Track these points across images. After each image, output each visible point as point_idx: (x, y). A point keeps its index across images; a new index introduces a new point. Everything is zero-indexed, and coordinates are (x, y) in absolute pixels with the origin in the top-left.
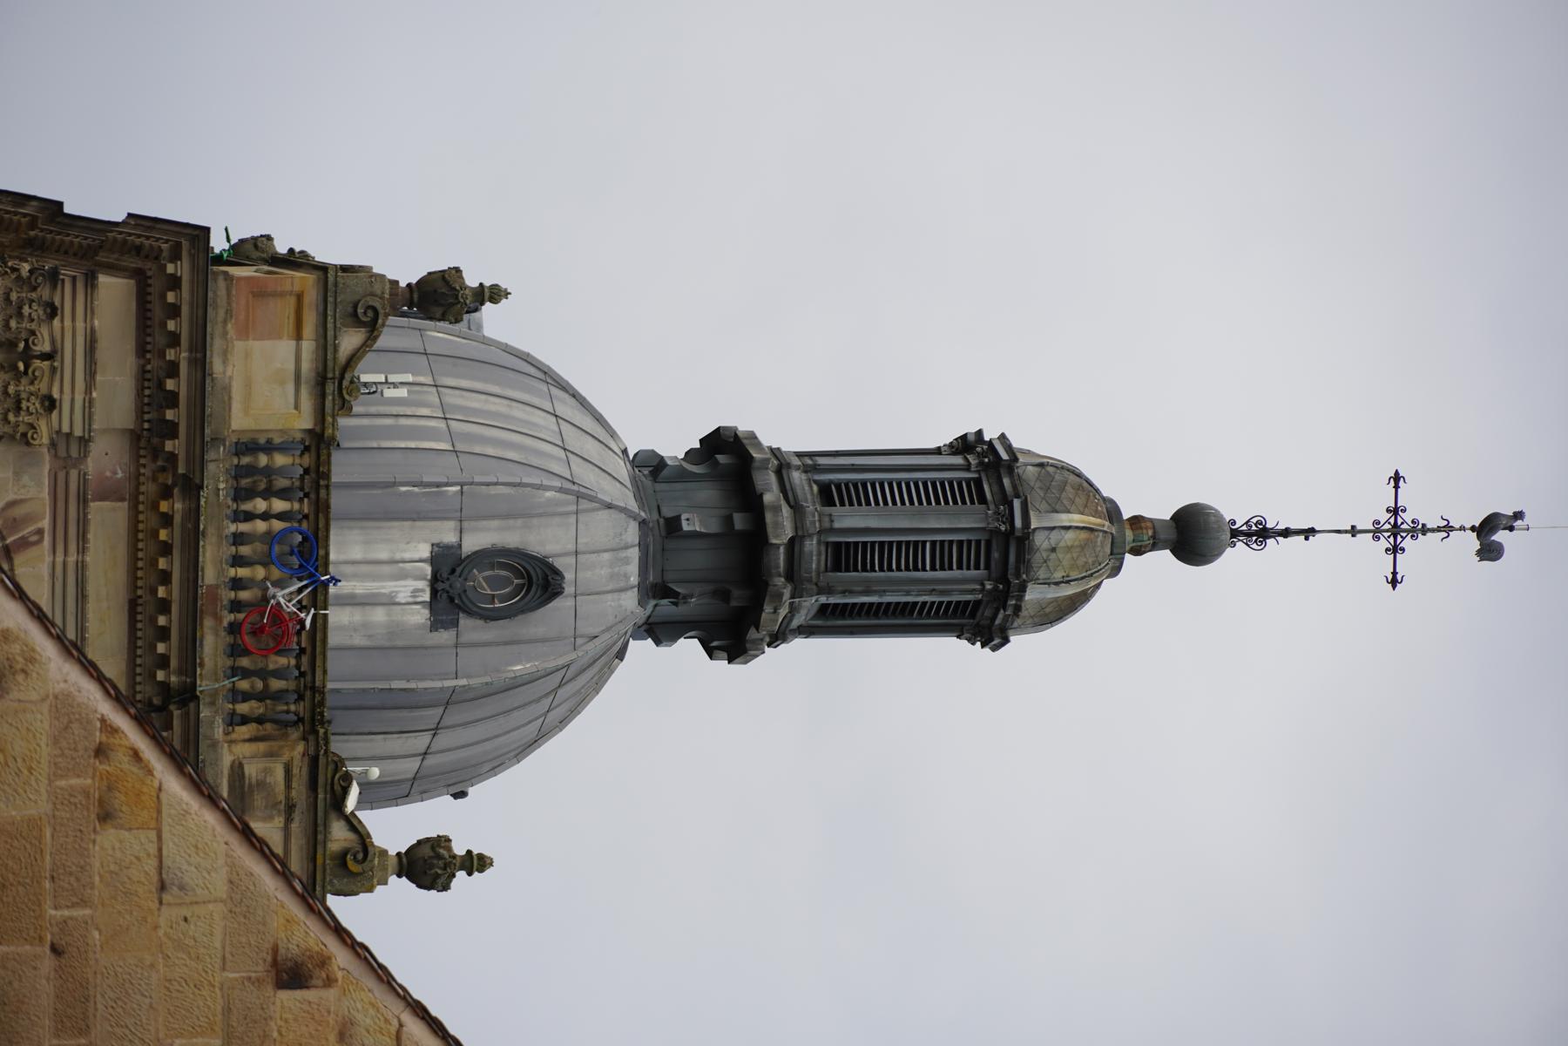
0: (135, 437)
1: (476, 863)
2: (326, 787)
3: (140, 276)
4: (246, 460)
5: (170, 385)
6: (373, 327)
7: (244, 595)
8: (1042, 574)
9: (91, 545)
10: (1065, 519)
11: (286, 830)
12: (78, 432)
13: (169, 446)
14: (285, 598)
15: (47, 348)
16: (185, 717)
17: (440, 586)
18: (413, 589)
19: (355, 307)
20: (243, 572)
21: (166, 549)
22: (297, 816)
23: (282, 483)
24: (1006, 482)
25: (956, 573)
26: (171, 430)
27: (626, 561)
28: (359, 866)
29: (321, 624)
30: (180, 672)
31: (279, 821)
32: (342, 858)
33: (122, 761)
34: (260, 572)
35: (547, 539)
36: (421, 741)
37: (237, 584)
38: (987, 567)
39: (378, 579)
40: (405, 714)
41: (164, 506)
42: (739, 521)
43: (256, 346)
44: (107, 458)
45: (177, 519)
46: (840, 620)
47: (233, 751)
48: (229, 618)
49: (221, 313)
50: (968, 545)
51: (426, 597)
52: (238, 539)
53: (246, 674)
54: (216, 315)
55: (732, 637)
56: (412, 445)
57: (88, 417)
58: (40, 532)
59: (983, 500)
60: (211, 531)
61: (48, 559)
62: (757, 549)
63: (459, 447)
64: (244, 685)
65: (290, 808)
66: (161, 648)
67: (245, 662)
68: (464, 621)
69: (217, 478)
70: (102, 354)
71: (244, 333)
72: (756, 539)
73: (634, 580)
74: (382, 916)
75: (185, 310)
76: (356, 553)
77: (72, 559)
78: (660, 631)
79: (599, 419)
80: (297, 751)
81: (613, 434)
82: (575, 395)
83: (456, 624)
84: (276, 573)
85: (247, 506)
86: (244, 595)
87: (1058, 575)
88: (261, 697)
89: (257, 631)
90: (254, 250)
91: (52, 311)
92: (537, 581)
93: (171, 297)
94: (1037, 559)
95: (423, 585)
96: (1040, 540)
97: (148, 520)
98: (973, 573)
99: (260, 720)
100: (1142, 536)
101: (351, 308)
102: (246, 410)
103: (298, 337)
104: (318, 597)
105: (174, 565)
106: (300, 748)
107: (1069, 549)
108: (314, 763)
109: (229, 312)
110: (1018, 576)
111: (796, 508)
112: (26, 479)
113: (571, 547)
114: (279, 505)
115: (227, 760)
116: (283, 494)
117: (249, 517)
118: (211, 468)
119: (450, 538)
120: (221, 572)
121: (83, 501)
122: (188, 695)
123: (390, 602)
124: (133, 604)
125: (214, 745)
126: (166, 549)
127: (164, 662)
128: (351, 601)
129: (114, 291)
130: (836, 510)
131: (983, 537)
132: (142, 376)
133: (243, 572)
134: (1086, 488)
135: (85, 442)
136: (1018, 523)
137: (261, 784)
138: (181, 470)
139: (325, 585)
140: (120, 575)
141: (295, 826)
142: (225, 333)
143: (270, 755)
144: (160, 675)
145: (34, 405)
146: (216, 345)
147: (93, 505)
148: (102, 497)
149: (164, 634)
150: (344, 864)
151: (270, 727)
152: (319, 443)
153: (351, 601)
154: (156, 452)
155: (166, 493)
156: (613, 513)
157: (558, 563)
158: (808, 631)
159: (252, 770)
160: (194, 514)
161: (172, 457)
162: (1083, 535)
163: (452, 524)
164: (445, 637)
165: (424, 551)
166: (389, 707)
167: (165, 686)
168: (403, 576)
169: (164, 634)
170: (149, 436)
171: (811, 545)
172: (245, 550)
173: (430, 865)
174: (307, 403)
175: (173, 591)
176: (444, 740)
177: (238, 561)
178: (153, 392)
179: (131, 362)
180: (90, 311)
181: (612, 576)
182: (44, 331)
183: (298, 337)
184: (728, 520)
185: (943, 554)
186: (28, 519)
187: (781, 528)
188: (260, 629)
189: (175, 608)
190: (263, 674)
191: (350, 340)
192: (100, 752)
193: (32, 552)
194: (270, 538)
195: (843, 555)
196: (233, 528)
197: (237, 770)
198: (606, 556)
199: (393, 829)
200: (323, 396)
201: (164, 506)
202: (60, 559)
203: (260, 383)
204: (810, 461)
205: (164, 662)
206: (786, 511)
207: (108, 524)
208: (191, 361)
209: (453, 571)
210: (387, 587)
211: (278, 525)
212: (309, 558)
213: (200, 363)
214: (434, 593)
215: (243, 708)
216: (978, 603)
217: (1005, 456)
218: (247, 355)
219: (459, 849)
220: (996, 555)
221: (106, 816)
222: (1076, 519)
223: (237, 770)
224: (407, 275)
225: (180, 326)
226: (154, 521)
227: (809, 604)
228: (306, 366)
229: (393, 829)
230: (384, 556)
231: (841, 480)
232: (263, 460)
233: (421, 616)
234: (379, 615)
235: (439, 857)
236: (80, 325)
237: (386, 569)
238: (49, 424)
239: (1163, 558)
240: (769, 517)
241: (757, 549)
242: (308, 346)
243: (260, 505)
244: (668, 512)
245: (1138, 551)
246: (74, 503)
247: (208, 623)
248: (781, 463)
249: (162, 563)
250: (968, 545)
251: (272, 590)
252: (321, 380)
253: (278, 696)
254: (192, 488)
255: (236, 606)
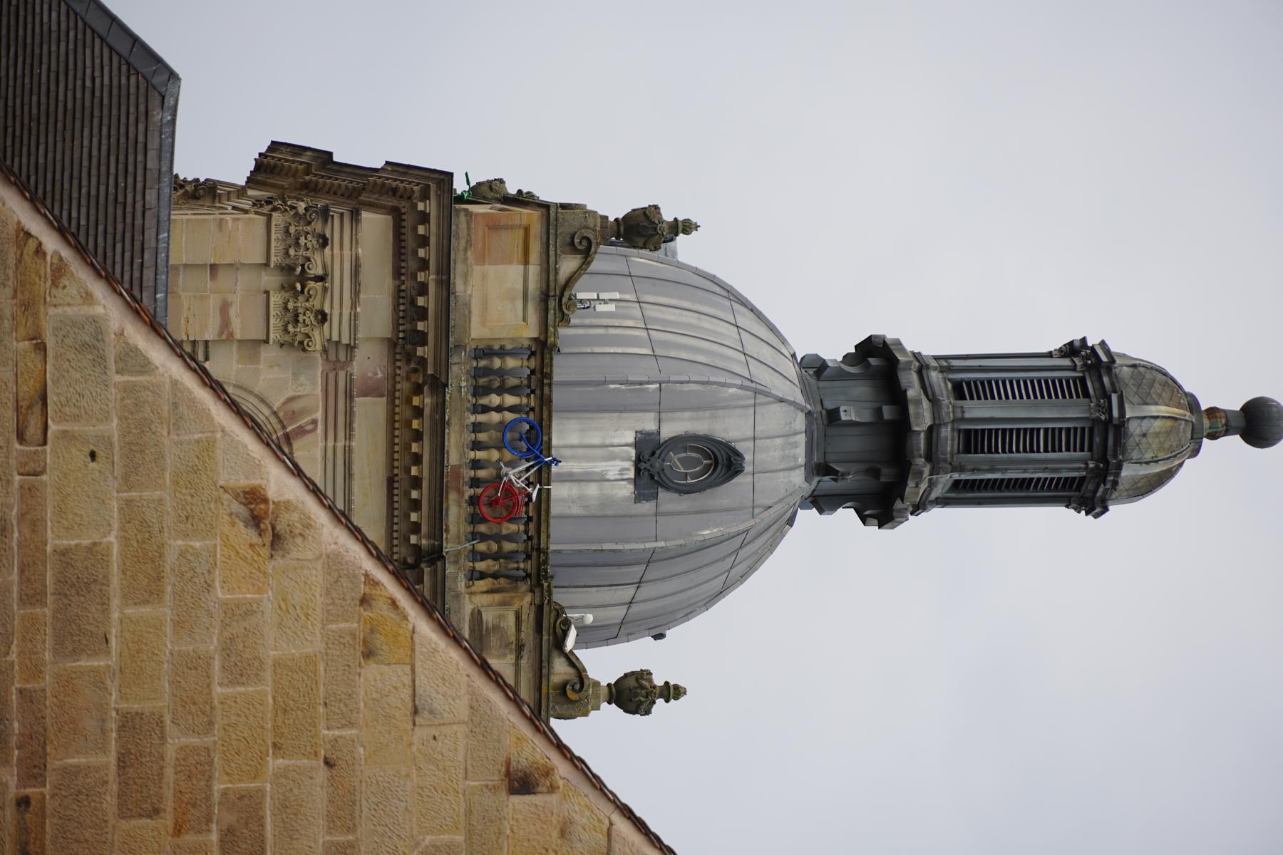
0: (392, 344)
1: (672, 692)
2: (549, 630)
3: (397, 214)
4: (483, 363)
5: (421, 301)
6: (587, 254)
7: (482, 474)
8: (1135, 455)
9: (356, 433)
10: (1153, 410)
11: (517, 665)
12: (345, 341)
13: (420, 351)
14: (515, 475)
15: (320, 272)
16: (434, 574)
17: (643, 466)
18: (620, 468)
19: (573, 238)
20: (480, 455)
21: (418, 436)
22: (525, 654)
23: (513, 381)
24: (1106, 380)
25: (1064, 455)
26: (422, 339)
27: (795, 445)
28: (575, 695)
29: (545, 497)
30: (429, 537)
31: (511, 658)
32: (562, 688)
33: (382, 607)
34: (495, 455)
35: (730, 428)
36: (628, 593)
37: (476, 464)
38: (1090, 449)
39: (592, 460)
40: (614, 570)
41: (416, 401)
42: (888, 413)
43: (491, 269)
44: (370, 362)
45: (427, 411)
46: (970, 492)
47: (472, 601)
48: (469, 492)
49: (463, 243)
50: (1075, 432)
51: (631, 475)
52: (477, 427)
53: (484, 538)
54: (458, 245)
55: (881, 507)
56: (620, 350)
57: (354, 329)
58: (314, 422)
59: (1086, 395)
60: (454, 421)
61: (321, 444)
62: (898, 436)
63: (658, 352)
64: (482, 547)
65: (520, 648)
66: (414, 517)
67: (482, 528)
68: (663, 495)
69: (459, 377)
70: (364, 277)
71: (482, 259)
72: (901, 427)
73: (801, 460)
74: (596, 735)
75: (433, 240)
76: (574, 439)
77: (340, 444)
78: (822, 502)
79: (773, 329)
80: (525, 601)
81: (784, 341)
82: (753, 310)
83: (655, 496)
84: (508, 455)
85: (484, 401)
86: (482, 474)
87: (1148, 456)
88: (496, 557)
89: (493, 503)
90: (489, 191)
91: (324, 242)
92: (723, 462)
93: (421, 230)
94: (1131, 442)
95: (629, 465)
96: (1134, 428)
97: (403, 411)
98: (1079, 454)
99: (495, 576)
100: (1216, 424)
101: (569, 239)
102: (483, 322)
103: (526, 262)
104: (542, 475)
105: (424, 449)
106: (528, 598)
107: (1157, 434)
108: (539, 610)
109: (469, 242)
110: (1115, 456)
111: (934, 401)
112: (302, 379)
113: (750, 434)
114: (510, 400)
115: (468, 608)
116: (514, 391)
117: (486, 409)
118: (455, 369)
119: (651, 426)
120: (463, 455)
121: (349, 396)
122: (436, 556)
123: (601, 479)
124: (391, 481)
125: (458, 596)
126: (418, 436)
127: (416, 528)
128: (570, 478)
129: (375, 225)
130: (967, 403)
131: (1087, 425)
132: (398, 294)
133: (480, 455)
134: (1171, 385)
135: (351, 348)
136: (1115, 413)
137: (496, 628)
138: (430, 372)
139: (549, 465)
140: (380, 458)
141: (524, 662)
142: (466, 259)
143: (503, 604)
144: (413, 539)
145: (310, 318)
146: (458, 269)
147: (358, 400)
148: (365, 394)
149: (416, 505)
150: (564, 693)
151: (503, 580)
152: (543, 348)
153: (570, 478)
154: (409, 357)
155: (418, 390)
156: (784, 406)
157: (740, 447)
158: (944, 502)
159: (488, 617)
160: (440, 407)
161: (423, 361)
162: (1169, 423)
163: (652, 415)
164: (647, 507)
165: (630, 437)
166: (601, 564)
167: (417, 548)
168: (612, 457)
169: (416, 505)
170: (404, 342)
171: (946, 432)
172: (482, 437)
173: (635, 694)
174: (533, 317)
175: (424, 471)
176: (646, 591)
177: (476, 446)
178: (407, 308)
179: (388, 283)
180: (355, 241)
181: (783, 458)
182: (317, 258)
183: (526, 262)
184: (879, 411)
185: (1054, 439)
186: (303, 412)
187: (922, 417)
188: (494, 501)
189: (425, 484)
190: (498, 538)
191: (568, 265)
192: (364, 601)
193: (308, 438)
194: (503, 427)
195: (973, 440)
196: (472, 418)
197: (477, 616)
198: (779, 441)
199: (604, 664)
200: (546, 310)
201: (416, 401)
202: (330, 444)
203: (494, 297)
204: (946, 363)
205: (416, 528)
206: (926, 404)
207: (370, 415)
208: (439, 283)
209: (653, 454)
210: (599, 467)
211: (509, 416)
212: (535, 444)
213: (445, 283)
214: (638, 471)
215: (481, 566)
216: (1082, 479)
217: (1104, 359)
218: (484, 277)
219: (659, 681)
220: (1097, 440)
221: (369, 654)
222: (1163, 410)
223: (477, 616)
224: (615, 211)
225: (430, 253)
226: (408, 413)
227: (945, 480)
228: (533, 286)
229: (604, 664)
230: (596, 441)
231: (971, 379)
232: (497, 363)
233: (627, 490)
234: (592, 490)
235: (642, 687)
236: (347, 252)
237: (599, 452)
238: (322, 334)
239: (1234, 442)
240: (912, 409)
241: (898, 436)
242: (534, 270)
243: (495, 400)
244: (829, 405)
245: (1213, 436)
246: (342, 396)
247: (453, 496)
248: (922, 365)
249: (415, 448)
250: (1075, 432)
251: (505, 470)
252: (545, 297)
253: (510, 556)
254: (439, 385)
255: (475, 482)
